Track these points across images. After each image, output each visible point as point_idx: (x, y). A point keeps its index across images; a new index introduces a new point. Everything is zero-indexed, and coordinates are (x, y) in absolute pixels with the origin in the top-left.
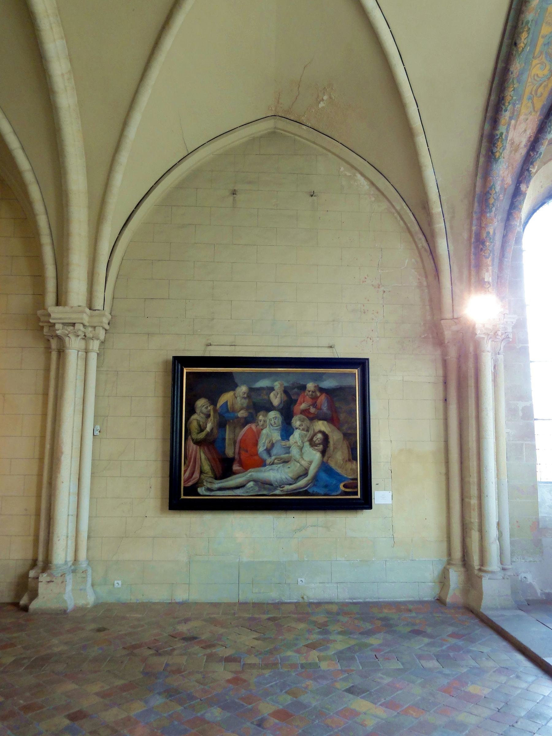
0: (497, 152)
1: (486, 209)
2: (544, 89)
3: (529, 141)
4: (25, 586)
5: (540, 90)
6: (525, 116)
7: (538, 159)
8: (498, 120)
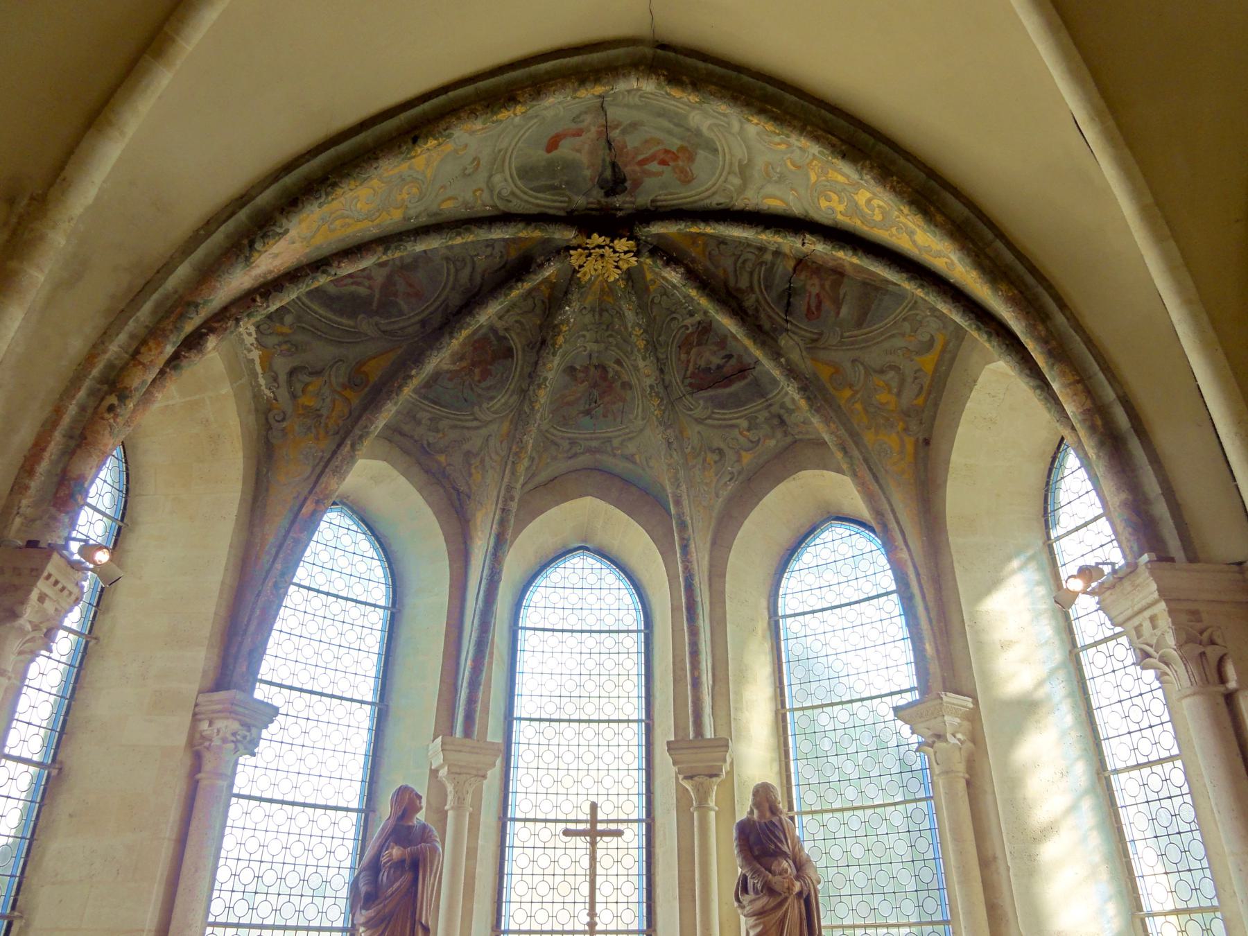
1: (172, 331)
4: (342, 930)
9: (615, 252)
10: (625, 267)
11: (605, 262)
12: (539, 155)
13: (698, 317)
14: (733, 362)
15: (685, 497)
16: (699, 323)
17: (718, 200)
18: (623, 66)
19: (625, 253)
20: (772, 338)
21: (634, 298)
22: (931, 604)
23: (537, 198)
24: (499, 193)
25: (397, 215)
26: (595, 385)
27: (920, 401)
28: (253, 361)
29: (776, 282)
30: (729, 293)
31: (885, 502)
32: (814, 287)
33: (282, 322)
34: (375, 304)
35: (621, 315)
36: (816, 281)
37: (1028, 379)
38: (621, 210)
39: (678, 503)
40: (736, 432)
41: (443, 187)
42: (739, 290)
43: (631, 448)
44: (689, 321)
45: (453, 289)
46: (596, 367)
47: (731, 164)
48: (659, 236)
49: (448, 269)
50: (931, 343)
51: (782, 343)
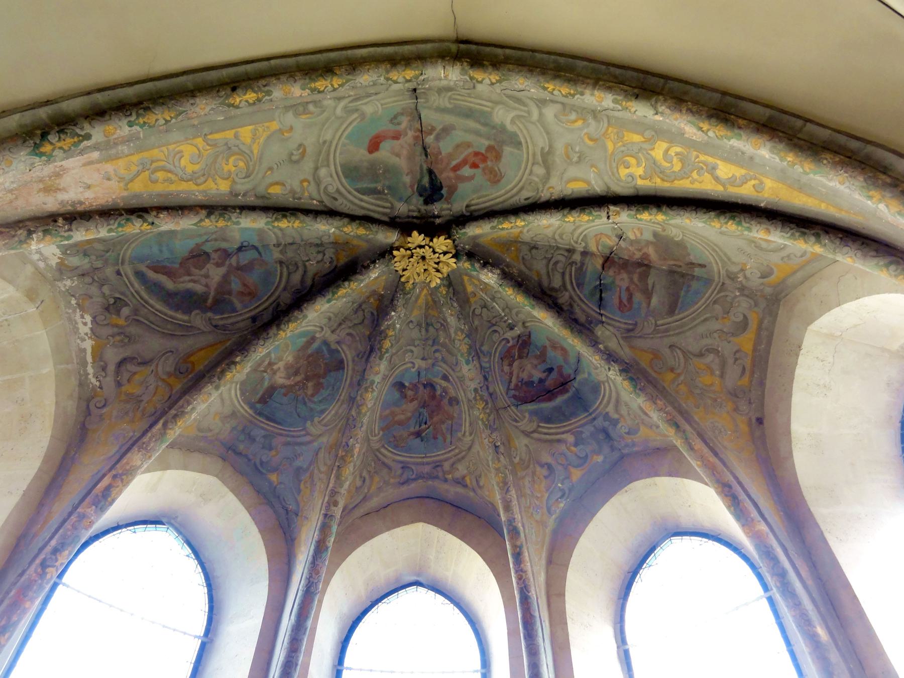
0: (51, 143)
2: (165, 181)
3: (74, 204)
5: (160, 175)
6: (112, 173)
7: (59, 239)
8: (107, 117)
9: (434, 252)
10: (445, 270)
11: (426, 263)
12: (361, 154)
13: (518, 331)
14: (554, 375)
15: (515, 503)
16: (519, 336)
17: (526, 195)
18: (431, 57)
19: (445, 253)
20: (589, 329)
21: (455, 304)
22: (810, 582)
23: (362, 200)
24: (326, 188)
25: (223, 187)
26: (424, 405)
27: (745, 380)
28: (84, 350)
29: (587, 279)
30: (543, 292)
31: (728, 474)
32: (622, 280)
33: (118, 313)
34: (210, 301)
35: (444, 326)
36: (625, 276)
37: (875, 261)
38: (438, 217)
39: (508, 508)
40: (563, 448)
41: (271, 169)
42: (553, 289)
43: (461, 470)
44: (509, 335)
45: (285, 289)
46: (425, 386)
47: (534, 155)
48: (475, 237)
49: (281, 274)
50: (744, 325)
51: (599, 333)
